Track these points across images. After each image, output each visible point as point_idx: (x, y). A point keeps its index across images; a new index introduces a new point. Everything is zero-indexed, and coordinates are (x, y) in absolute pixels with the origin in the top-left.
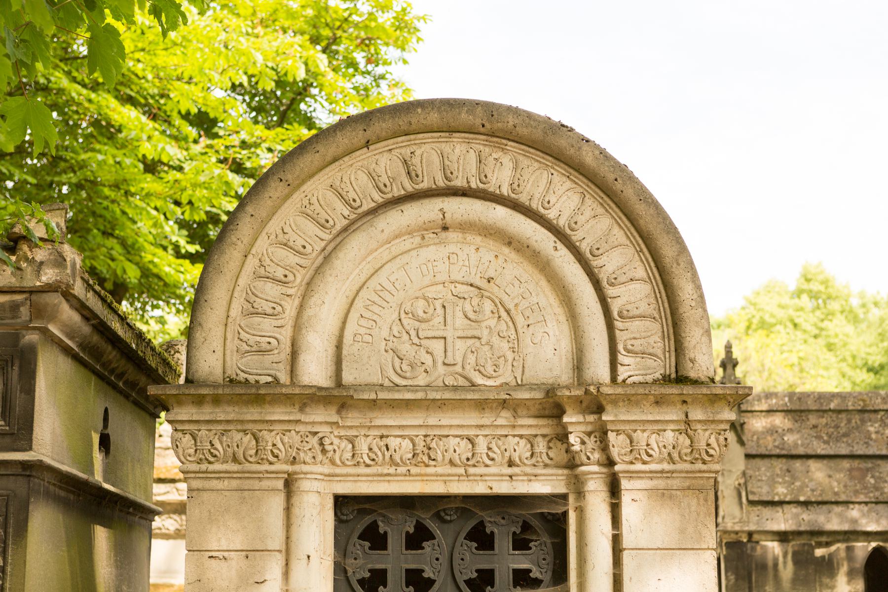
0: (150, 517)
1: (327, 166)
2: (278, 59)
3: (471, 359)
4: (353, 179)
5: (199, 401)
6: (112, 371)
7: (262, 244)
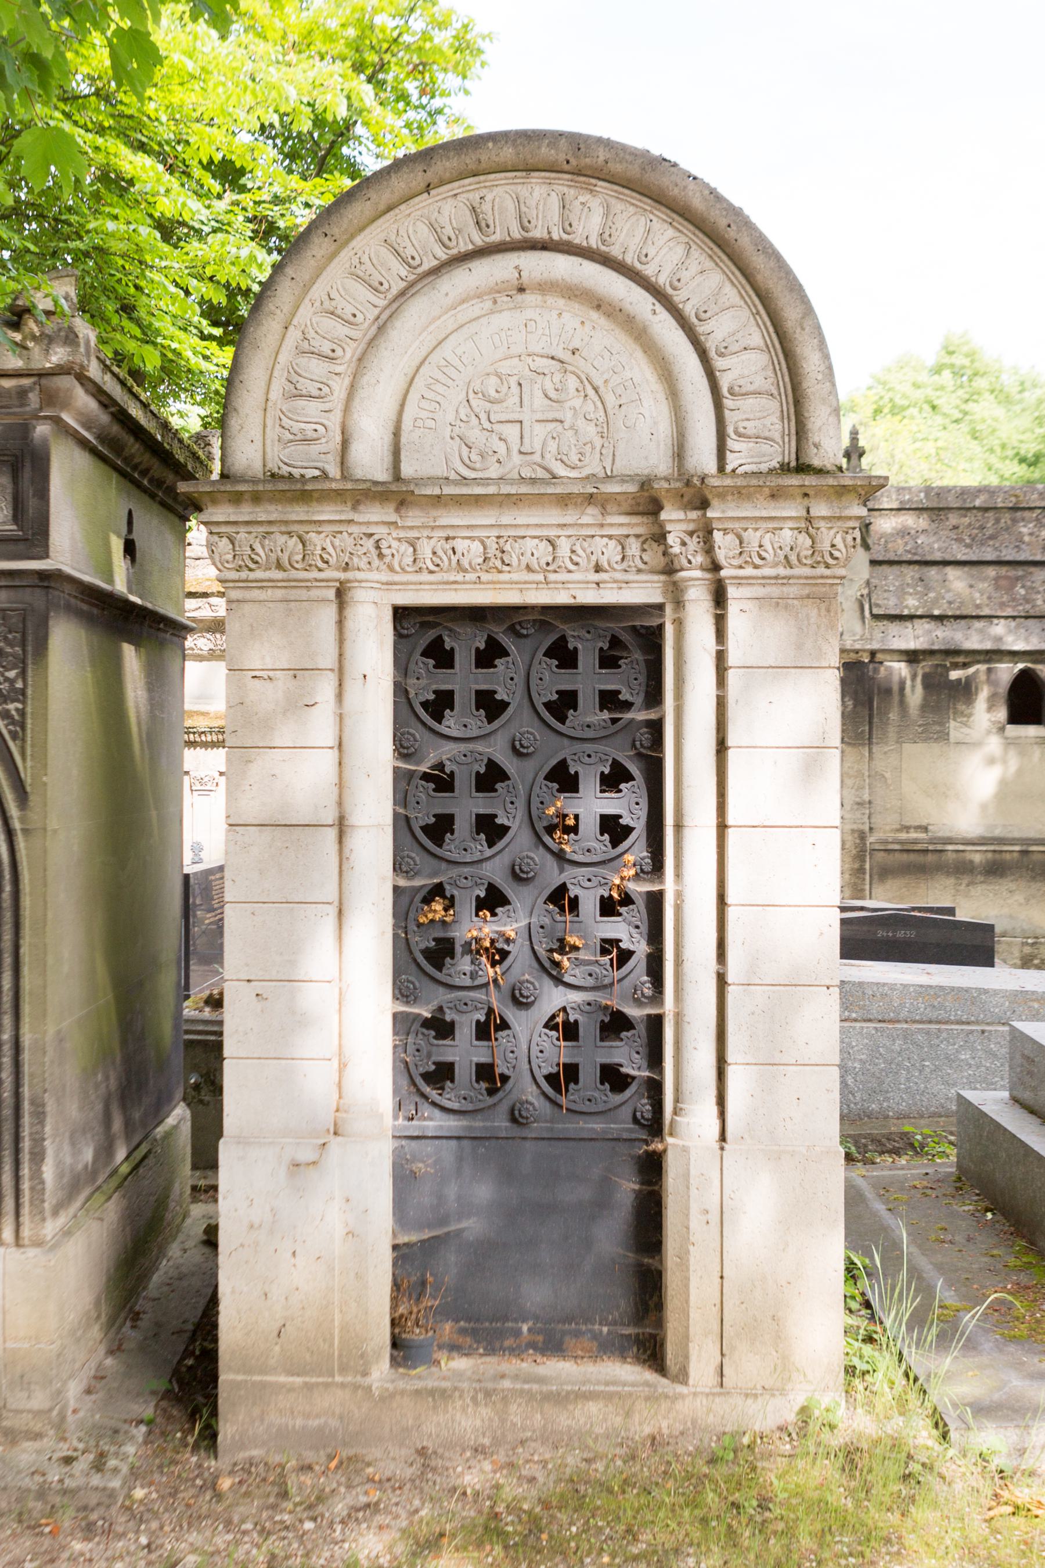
0: (183, 633)
1: (380, 216)
2: (315, 93)
3: (552, 446)
4: (411, 231)
5: (236, 499)
6: (135, 467)
7: (305, 313)
